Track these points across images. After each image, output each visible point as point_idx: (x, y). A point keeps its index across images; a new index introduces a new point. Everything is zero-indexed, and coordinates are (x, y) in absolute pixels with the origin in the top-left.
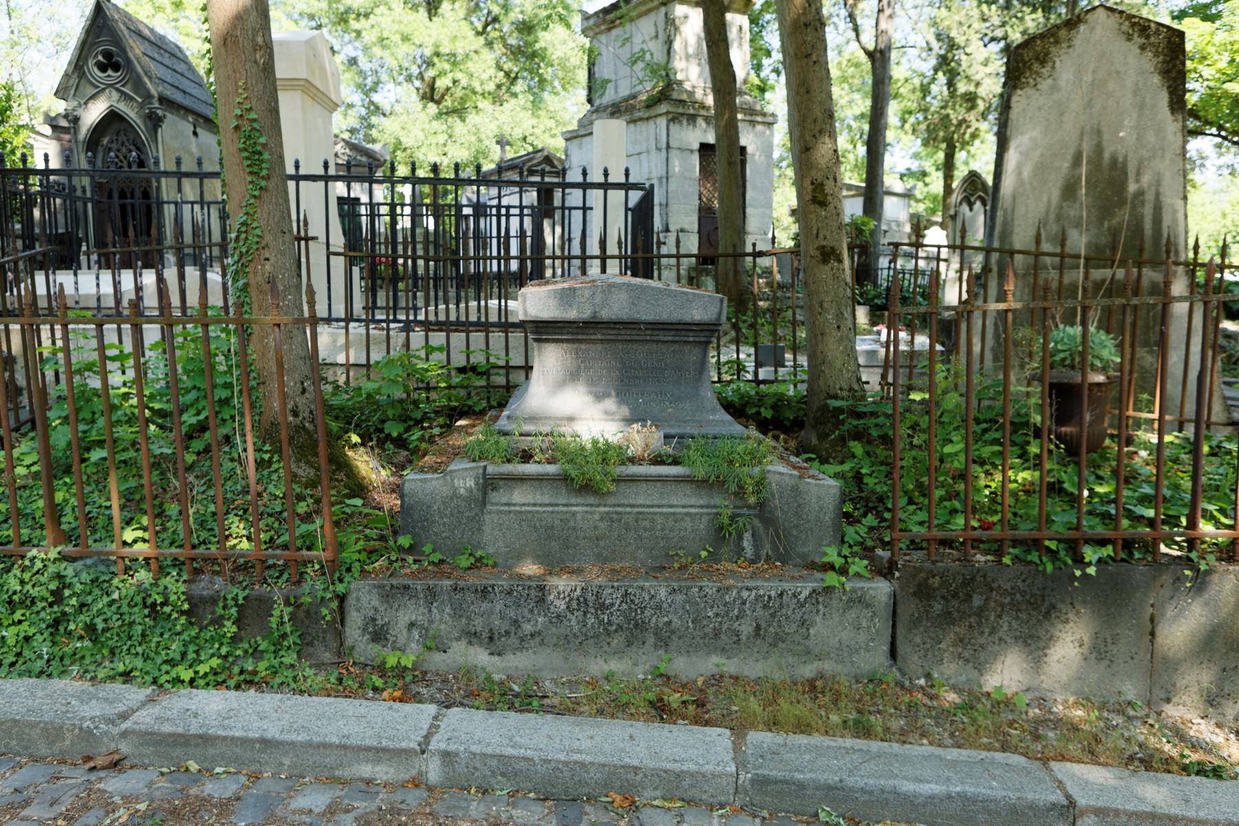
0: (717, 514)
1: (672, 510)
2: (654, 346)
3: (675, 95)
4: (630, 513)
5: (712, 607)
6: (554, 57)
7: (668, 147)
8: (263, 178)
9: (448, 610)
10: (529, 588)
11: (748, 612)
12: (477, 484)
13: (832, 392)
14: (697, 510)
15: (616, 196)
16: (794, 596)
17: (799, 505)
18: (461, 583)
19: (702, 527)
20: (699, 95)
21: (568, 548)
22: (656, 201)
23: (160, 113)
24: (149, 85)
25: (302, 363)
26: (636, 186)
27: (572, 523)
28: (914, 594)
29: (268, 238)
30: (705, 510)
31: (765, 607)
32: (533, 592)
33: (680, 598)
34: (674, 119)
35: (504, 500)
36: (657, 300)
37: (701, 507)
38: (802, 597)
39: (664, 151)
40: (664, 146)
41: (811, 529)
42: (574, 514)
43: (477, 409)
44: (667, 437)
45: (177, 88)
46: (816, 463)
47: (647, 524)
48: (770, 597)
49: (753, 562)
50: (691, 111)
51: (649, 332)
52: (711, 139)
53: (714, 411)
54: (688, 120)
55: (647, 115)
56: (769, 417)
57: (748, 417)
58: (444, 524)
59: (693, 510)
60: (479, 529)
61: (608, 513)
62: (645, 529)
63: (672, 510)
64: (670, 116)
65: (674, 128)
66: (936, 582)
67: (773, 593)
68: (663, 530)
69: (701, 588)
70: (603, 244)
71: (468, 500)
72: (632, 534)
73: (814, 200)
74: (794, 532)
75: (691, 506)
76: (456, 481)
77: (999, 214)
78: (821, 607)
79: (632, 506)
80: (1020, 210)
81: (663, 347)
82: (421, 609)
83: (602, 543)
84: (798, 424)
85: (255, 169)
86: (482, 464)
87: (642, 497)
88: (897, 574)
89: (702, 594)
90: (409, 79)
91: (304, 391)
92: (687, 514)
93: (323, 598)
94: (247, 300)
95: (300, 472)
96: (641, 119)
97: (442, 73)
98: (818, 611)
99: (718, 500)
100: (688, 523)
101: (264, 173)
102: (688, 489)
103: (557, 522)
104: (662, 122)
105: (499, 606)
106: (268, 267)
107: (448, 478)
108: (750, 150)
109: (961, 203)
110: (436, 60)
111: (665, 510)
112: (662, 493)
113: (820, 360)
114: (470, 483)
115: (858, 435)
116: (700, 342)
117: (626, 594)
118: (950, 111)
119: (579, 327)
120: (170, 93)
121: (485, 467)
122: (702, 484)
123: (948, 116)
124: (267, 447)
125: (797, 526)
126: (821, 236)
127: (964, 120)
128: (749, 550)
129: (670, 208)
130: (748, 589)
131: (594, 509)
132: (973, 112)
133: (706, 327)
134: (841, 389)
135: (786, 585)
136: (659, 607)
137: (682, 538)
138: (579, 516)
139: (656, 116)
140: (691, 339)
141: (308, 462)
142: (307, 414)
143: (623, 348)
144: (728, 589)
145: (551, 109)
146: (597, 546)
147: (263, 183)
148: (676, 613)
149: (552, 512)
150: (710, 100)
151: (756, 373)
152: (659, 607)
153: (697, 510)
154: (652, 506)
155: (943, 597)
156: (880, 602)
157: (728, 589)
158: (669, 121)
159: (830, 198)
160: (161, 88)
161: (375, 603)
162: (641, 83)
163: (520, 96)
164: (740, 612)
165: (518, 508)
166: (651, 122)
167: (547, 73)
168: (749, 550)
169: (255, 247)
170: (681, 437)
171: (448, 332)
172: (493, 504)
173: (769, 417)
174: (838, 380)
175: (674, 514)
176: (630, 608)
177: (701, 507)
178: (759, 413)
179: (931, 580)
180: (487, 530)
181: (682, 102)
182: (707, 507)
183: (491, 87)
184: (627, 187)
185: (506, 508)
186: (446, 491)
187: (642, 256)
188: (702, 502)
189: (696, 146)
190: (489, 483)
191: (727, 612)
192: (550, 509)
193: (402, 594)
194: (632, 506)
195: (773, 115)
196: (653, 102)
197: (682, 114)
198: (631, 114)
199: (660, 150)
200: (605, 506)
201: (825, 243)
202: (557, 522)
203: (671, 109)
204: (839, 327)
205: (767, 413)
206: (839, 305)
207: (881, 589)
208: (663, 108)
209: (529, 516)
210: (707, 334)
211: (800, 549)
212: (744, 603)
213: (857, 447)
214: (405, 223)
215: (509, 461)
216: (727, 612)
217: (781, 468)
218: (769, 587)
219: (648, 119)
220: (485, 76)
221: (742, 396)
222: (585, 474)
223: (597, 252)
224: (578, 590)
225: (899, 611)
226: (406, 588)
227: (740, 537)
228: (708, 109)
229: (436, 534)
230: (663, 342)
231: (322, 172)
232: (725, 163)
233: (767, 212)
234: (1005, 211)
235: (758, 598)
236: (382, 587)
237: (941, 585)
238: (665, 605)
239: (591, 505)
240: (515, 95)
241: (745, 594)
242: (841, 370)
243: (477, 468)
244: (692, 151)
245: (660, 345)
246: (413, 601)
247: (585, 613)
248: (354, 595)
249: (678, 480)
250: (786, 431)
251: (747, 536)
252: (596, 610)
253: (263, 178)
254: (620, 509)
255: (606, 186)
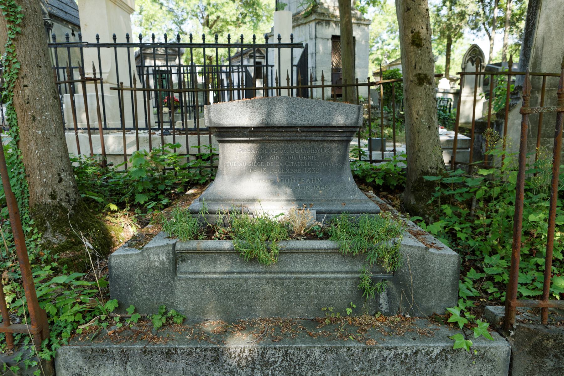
0: (359, 278)
1: (323, 276)
2: (308, 143)
3: (319, 10)
4: (290, 279)
5: (358, 363)
6: (263, 4)
7: (316, 37)
8: (19, 25)
9: (140, 368)
10: (206, 350)
11: (388, 367)
12: (168, 258)
13: (425, 170)
14: (343, 275)
15: (286, 52)
16: (427, 354)
17: (425, 271)
18: (150, 347)
19: (347, 288)
20: (331, 10)
21: (242, 305)
22: (310, 65)
23: (50, 22)
24: (43, 7)
25: (59, 160)
26: (299, 45)
27: (244, 287)
28: (530, 352)
29: (26, 70)
30: (350, 275)
31: (402, 363)
32: (209, 354)
33: (331, 356)
34: (319, 22)
35: (191, 269)
36: (311, 109)
37: (347, 272)
38: (434, 354)
39: (314, 40)
40: (314, 37)
41: (434, 289)
42: (246, 280)
43: (201, 182)
44: (318, 213)
45: (61, 10)
46: (423, 224)
47: (304, 286)
48: (406, 355)
49: (388, 314)
50: (327, 19)
51: (303, 134)
52: (338, 32)
53: (353, 192)
54: (326, 23)
55: (305, 22)
56: (381, 184)
57: (367, 184)
58: (144, 289)
59: (340, 275)
60: (172, 292)
61: (272, 279)
62: (302, 291)
63: (323, 276)
64: (317, 21)
65: (319, 27)
66: (550, 343)
67: (409, 352)
68: (316, 291)
69: (349, 349)
70: (278, 80)
71: (162, 271)
72: (292, 294)
73: (413, 43)
74: (421, 292)
75: (339, 272)
76: (151, 256)
77: (533, 51)
78: (449, 362)
79: (292, 273)
80: (547, 48)
81: (315, 145)
82: (118, 368)
83: (268, 301)
84: (400, 188)
85: (12, 19)
86: (173, 242)
87: (299, 266)
88: (512, 333)
89: (350, 353)
90: (197, 16)
91: (61, 180)
92: (335, 279)
93: (29, 366)
94: (14, 116)
95: (54, 240)
96: (302, 24)
97: (212, 13)
98: (446, 366)
99: (359, 267)
100: (336, 286)
101: (18, 21)
102: (335, 258)
103: (233, 286)
104: (313, 24)
105: (181, 365)
106: (27, 91)
107: (145, 254)
108: (357, 38)
109: (468, 62)
110: (208, 7)
111: (318, 276)
112: (315, 262)
113: (417, 150)
114: (163, 257)
115: (445, 200)
116: (343, 141)
117: (286, 354)
118: (452, 21)
119: (250, 131)
120: (55, 11)
121: (174, 245)
122: (350, 256)
123: (451, 24)
124: (32, 222)
125: (423, 287)
126: (418, 67)
127: (458, 26)
128: (384, 306)
129: (317, 69)
130: (388, 349)
131: (261, 275)
132: (463, 22)
133: (347, 129)
134: (431, 168)
135: (420, 345)
136: (314, 364)
137: (331, 297)
138: (250, 282)
139: (309, 22)
140: (336, 138)
141: (62, 232)
142: (64, 195)
143: (285, 147)
144: (371, 349)
145: (262, 29)
146: (265, 304)
147: (18, 29)
148: (328, 367)
149: (228, 279)
150: (337, 13)
151: (371, 156)
152: (314, 364)
153: (343, 275)
154: (308, 273)
155: (555, 356)
156: (499, 358)
157: (371, 349)
158: (316, 24)
159: (424, 42)
160: (50, 9)
161: (80, 363)
162: (302, 5)
163: (248, 23)
164: (381, 367)
165: (202, 276)
166: (307, 25)
167: (260, 12)
168: (384, 306)
169: (15, 77)
170: (330, 212)
171: (187, 134)
172: (182, 273)
173: (381, 184)
174: (429, 163)
175: (325, 279)
176: (290, 365)
177: (347, 272)
178: (374, 181)
179: (546, 342)
180: (178, 292)
181: (323, 14)
182: (351, 272)
183: (234, 19)
184: (292, 46)
185: (192, 276)
186: (144, 264)
187: (303, 88)
188: (347, 269)
189: (330, 37)
190: (177, 257)
191: (371, 367)
192: (227, 276)
193: (101, 356)
194: (292, 273)
195: (369, 20)
196: (308, 14)
197: (323, 20)
198: (297, 22)
199: (312, 39)
200: (270, 273)
201: (420, 72)
202: (233, 286)
203: (317, 17)
204: (429, 127)
205: (379, 182)
206: (429, 113)
207: (501, 347)
208: (313, 17)
209: (211, 282)
210: (348, 134)
211: (425, 304)
212: (385, 360)
213: (448, 209)
214: (187, 78)
215: (196, 238)
216: (371, 367)
217: (412, 241)
218: (406, 346)
219: (305, 23)
220: (231, 13)
221: (363, 171)
222: (257, 243)
223: (275, 85)
224: (247, 351)
225: (515, 365)
226: (104, 351)
227: (377, 296)
228: (336, 17)
229: (138, 297)
230: (314, 141)
231: (112, 42)
232: (344, 44)
233: (366, 70)
234: (537, 49)
235: (397, 356)
236: (84, 351)
237: (554, 347)
238: (319, 362)
239: (260, 273)
240: (245, 23)
241: (386, 353)
242: (431, 156)
243: (167, 245)
244: (328, 39)
245: (312, 143)
246: (111, 361)
247: (253, 369)
248: (62, 358)
249: (327, 252)
250: (391, 192)
251: (383, 295)
252: (262, 366)
253: (19, 25)
254: (282, 275)
255: (279, 46)
